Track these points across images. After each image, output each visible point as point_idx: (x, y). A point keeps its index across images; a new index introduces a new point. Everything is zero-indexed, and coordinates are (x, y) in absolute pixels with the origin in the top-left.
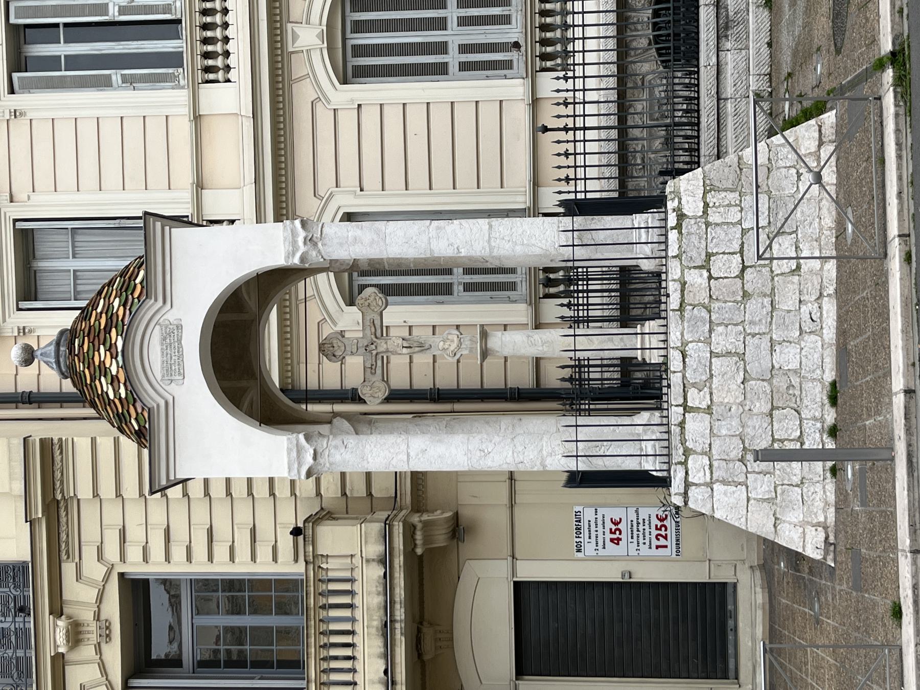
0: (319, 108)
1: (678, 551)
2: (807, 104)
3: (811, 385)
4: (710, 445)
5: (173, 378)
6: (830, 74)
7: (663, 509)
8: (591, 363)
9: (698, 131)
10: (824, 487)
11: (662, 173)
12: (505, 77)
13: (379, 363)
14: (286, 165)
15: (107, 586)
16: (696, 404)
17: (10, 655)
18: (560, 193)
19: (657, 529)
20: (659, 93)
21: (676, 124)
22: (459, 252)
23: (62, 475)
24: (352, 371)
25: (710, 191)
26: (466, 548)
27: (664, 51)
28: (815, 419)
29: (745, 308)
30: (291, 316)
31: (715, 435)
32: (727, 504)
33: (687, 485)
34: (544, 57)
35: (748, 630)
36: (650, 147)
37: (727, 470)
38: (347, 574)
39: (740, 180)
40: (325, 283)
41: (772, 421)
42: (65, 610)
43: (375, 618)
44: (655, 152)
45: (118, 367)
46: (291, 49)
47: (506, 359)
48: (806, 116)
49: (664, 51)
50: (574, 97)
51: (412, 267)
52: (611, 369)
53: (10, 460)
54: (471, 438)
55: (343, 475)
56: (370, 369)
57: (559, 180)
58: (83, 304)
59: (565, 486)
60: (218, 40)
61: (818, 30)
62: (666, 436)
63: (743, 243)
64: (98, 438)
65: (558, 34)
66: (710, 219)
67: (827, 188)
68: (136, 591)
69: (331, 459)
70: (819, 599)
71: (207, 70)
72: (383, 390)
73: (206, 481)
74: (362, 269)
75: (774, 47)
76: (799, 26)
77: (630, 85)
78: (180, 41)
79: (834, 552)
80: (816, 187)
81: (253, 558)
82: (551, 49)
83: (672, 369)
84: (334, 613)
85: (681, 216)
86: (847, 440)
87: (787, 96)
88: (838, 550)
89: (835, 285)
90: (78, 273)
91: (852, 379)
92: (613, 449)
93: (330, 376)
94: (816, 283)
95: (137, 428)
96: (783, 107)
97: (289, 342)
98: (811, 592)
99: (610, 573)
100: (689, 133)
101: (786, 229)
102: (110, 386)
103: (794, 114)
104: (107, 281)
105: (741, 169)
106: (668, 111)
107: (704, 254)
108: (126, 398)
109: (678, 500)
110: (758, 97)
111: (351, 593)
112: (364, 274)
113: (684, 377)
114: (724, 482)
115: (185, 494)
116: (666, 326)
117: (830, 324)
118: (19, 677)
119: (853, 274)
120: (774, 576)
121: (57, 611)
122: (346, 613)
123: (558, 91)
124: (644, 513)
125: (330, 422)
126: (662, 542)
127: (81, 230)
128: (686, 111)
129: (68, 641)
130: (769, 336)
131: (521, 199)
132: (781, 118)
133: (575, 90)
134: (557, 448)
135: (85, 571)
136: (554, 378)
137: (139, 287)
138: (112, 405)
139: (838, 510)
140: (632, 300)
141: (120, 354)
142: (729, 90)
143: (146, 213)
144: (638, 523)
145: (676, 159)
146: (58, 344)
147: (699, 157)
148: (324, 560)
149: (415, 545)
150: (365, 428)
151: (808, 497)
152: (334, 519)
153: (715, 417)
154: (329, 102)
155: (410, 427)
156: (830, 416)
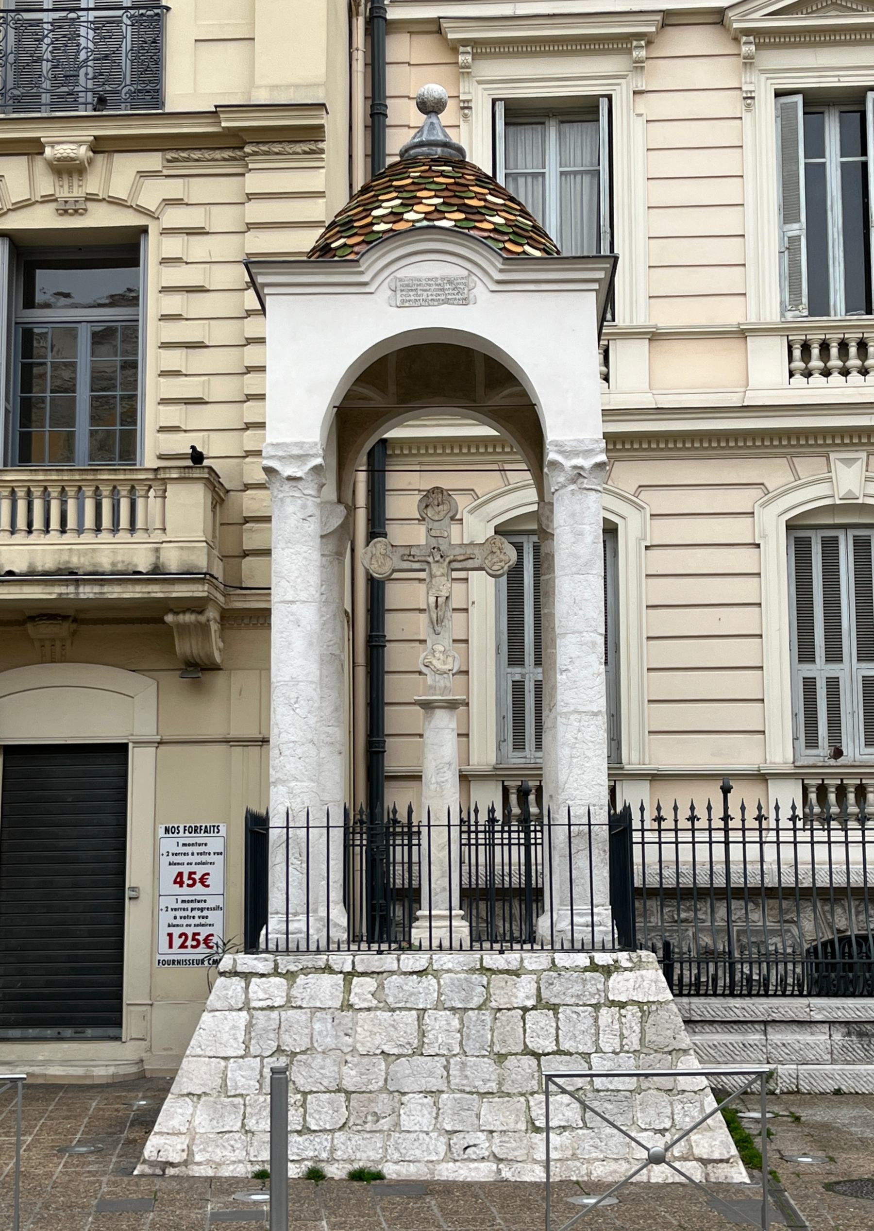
0: (756, 493)
1: (165, 962)
2: (758, 1142)
3: (379, 1145)
4: (300, 1007)
5: (398, 292)
6: (798, 1175)
7: (220, 943)
8: (415, 849)
9: (723, 995)
10: (240, 1162)
11: (667, 946)
12: (795, 739)
13: (416, 566)
14: (679, 449)
15: (131, 210)
16: (355, 989)
17: (44, 86)
18: (642, 809)
19: (195, 934)
20: (774, 943)
21: (732, 965)
22: (562, 672)
23: (277, 154)
24: (408, 532)
25: (642, 1011)
26: (172, 680)
27: (829, 950)
28: (333, 1150)
29: (484, 1056)
30: (482, 454)
31: (313, 1014)
32: (219, 1028)
33: (247, 976)
34: (822, 790)
35: (59, 1056)
36: (703, 930)
37: (266, 1030)
38: (140, 524)
39: (656, 1051)
40: (522, 500)
41: (330, 1092)
42: (100, 157)
43: (82, 560)
44: (695, 937)
45: (414, 221)
46: (832, 456)
47: (421, 736)
48: (743, 1142)
49: (829, 950)
50: (768, 829)
51: (544, 611)
52: (406, 875)
53: (297, 86)
54: (314, 686)
55: (268, 519)
56: (408, 554)
57: (659, 809)
58: (501, 180)
59: (247, 811)
60: (844, 362)
61: (858, 1159)
62: (313, 947)
63: (571, 1054)
64: (324, 200)
65: (853, 809)
66: (604, 1011)
67: (645, 1171)
68: (122, 250)
69: (288, 500)
70: (92, 1152)
71: (806, 348)
72: (380, 571)
73: (261, 341)
74: (543, 545)
75: (834, 1097)
76: (863, 1133)
77: (785, 904)
78: (843, 312)
79: (154, 1175)
80: (644, 1155)
81: (164, 401)
82: (830, 801)
83: (403, 957)
84: (89, 506)
85: (608, 971)
86: (303, 1195)
87: (768, 1115)
88: (156, 1180)
89: (513, 1179)
90: (540, 179)
91: (384, 1203)
92: (297, 877)
93: (401, 505)
94: (516, 1153)
95: (333, 246)
96: (755, 1110)
97: (448, 451)
98: (102, 1141)
99: (136, 872)
100: (721, 983)
101: (589, 1114)
102: (390, 210)
103: (745, 1124)
104: (529, 210)
105: (670, 1053)
106: (750, 954)
107: (557, 1001)
108: (373, 232)
109: (226, 963)
110: (769, 1076)
111: (115, 528)
112: (537, 549)
113: (392, 973)
114: (249, 1026)
115: (249, 313)
116: (461, 950)
117: (461, 1172)
118: (14, 98)
119: (527, 1205)
120: (129, 1091)
121: (99, 146)
122: (89, 521)
123: (777, 808)
124: (215, 917)
125: (339, 501)
126: (177, 942)
127: (598, 182)
128: (749, 979)
129: (59, 160)
130: (445, 1089)
131: (635, 758)
132: (739, 1107)
133: (778, 830)
134: (299, 800)
135: (149, 183)
136: (397, 798)
137: (518, 249)
138: (364, 214)
139: (210, 1180)
140: (498, 905)
141: (431, 223)
142: (776, 1036)
143: (616, 259)
144: (202, 910)
145: (686, 966)
146: (446, 145)
147: (689, 995)
148: (160, 493)
149: (177, 613)
150: (331, 547)
151: (228, 1140)
152: (214, 507)
153: (337, 1013)
154: (764, 505)
155: (333, 607)
156: (336, 1171)
